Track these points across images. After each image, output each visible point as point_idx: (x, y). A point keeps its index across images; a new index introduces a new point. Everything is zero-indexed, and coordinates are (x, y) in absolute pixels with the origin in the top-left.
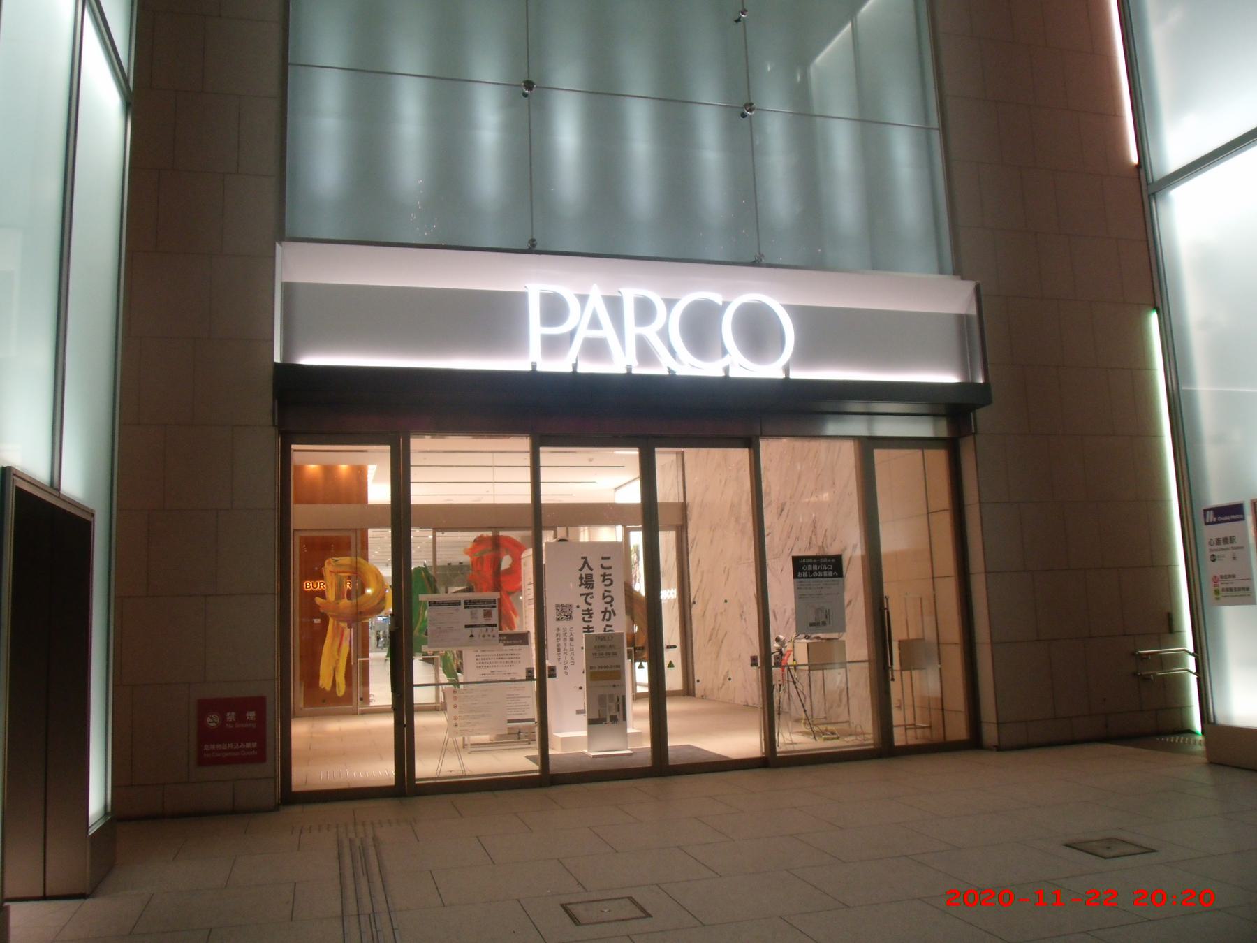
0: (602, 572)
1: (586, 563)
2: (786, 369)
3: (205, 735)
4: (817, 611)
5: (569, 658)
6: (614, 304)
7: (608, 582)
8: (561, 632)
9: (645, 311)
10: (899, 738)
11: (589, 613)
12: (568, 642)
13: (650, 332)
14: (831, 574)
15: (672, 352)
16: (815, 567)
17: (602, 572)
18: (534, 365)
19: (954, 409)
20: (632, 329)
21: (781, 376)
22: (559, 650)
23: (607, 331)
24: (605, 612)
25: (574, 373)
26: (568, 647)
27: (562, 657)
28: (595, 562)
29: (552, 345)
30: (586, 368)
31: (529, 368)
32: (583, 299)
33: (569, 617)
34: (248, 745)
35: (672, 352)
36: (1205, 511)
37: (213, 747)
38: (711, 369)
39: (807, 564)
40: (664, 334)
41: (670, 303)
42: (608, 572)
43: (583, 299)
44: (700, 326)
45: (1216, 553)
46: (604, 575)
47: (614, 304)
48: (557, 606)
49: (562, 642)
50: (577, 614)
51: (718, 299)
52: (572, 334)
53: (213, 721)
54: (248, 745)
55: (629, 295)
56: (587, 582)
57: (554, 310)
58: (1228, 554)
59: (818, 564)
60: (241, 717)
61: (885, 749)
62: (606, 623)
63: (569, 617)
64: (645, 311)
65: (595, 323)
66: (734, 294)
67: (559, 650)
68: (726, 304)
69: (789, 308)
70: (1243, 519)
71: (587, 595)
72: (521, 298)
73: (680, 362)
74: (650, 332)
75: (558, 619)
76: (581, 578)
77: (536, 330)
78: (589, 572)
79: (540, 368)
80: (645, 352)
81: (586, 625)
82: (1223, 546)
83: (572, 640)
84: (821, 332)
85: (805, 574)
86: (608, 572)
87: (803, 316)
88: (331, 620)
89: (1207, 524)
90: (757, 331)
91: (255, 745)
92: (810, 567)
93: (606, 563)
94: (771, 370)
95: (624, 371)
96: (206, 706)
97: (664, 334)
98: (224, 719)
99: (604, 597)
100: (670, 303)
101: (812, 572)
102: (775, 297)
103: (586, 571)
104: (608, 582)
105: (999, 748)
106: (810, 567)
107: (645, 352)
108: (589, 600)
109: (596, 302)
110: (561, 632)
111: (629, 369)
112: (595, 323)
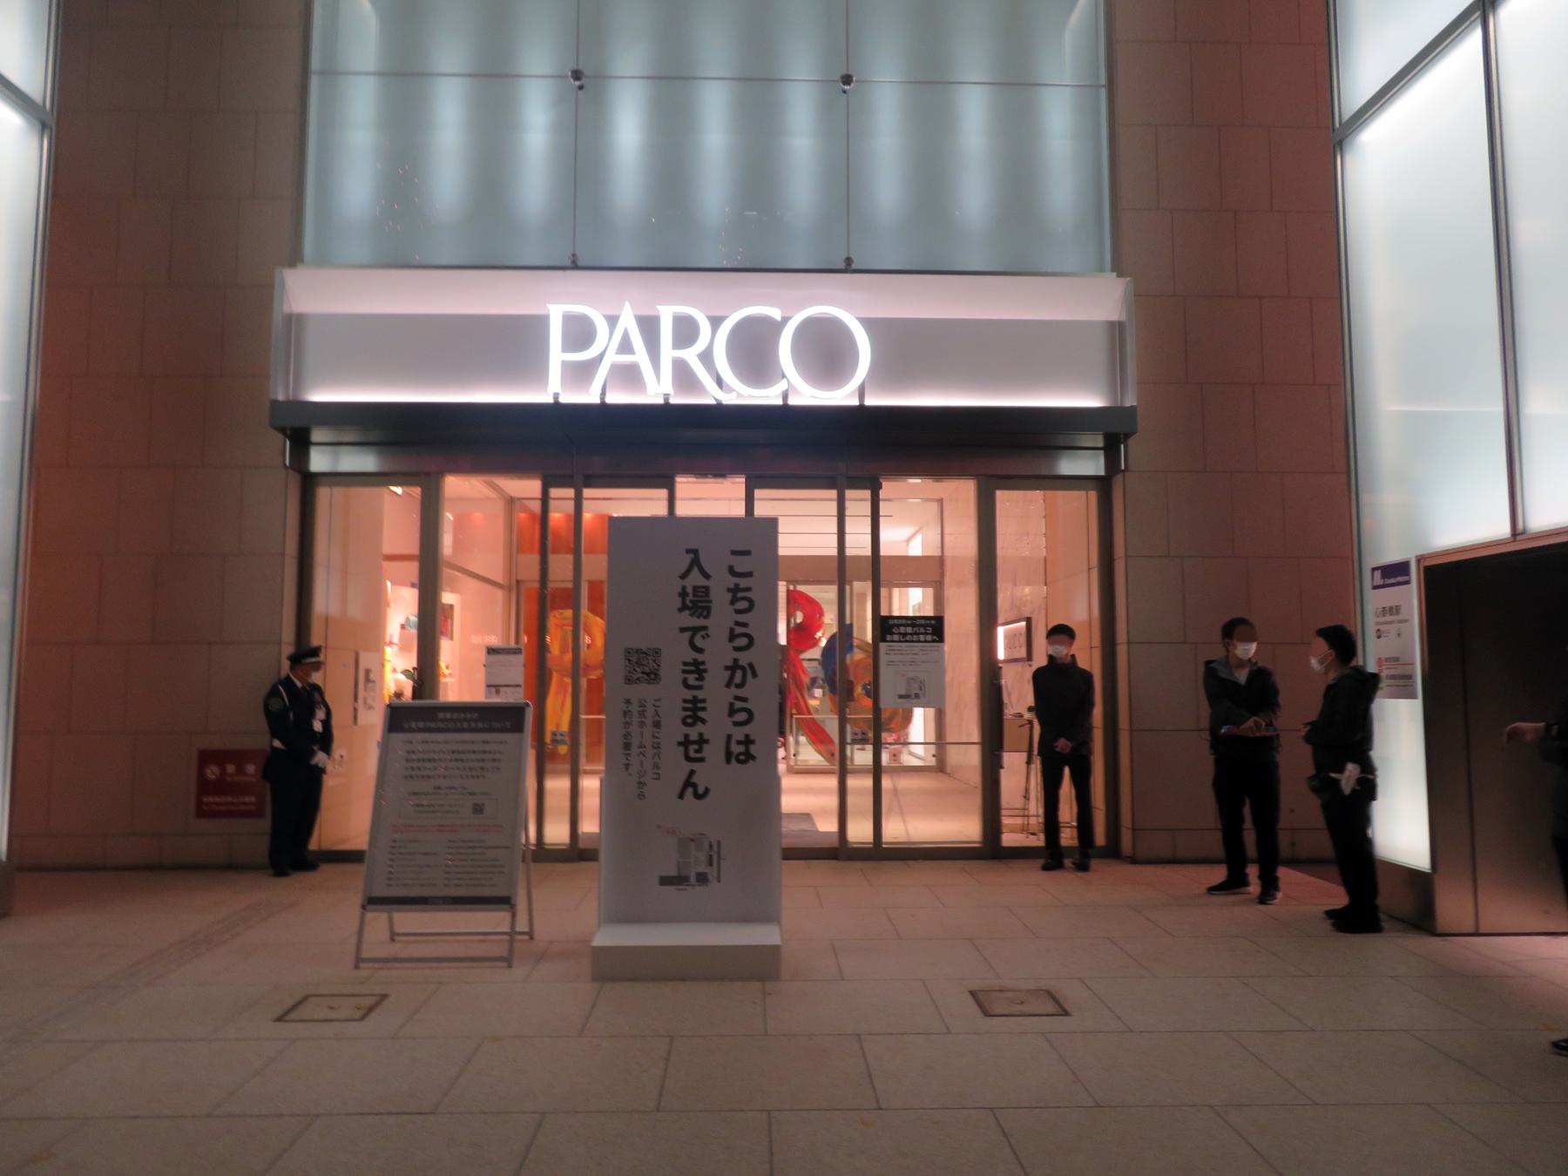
1: (695, 562)
2: (861, 392)
3: (205, 787)
4: (910, 680)
6: (649, 326)
7: (743, 605)
8: (634, 708)
9: (686, 332)
10: (1009, 839)
12: (649, 730)
13: (690, 355)
14: (929, 638)
15: (720, 382)
16: (909, 630)
18: (556, 396)
19: (1112, 429)
20: (668, 352)
21: (855, 402)
22: (627, 746)
24: (734, 667)
26: (648, 741)
28: (716, 562)
29: (580, 373)
30: (616, 398)
31: (550, 400)
32: (612, 321)
33: (653, 676)
34: (247, 799)
35: (720, 382)
36: (1374, 569)
37: (211, 799)
38: (769, 396)
39: (899, 626)
40: (706, 357)
41: (716, 322)
42: (743, 583)
43: (612, 321)
44: (753, 349)
45: (1382, 627)
46: (735, 590)
47: (649, 326)
48: (628, 652)
49: (634, 730)
50: (671, 671)
51: (776, 314)
52: (601, 356)
53: (212, 772)
54: (247, 799)
55: (666, 315)
56: (697, 602)
57: (580, 332)
58: (1393, 628)
59: (913, 625)
60: (241, 771)
61: (991, 850)
62: (734, 691)
63: (653, 676)
64: (686, 332)
65: (626, 346)
66: (790, 308)
67: (627, 746)
68: (785, 320)
69: (867, 323)
70: (1408, 582)
72: (542, 322)
73: (730, 390)
74: (690, 355)
75: (628, 681)
76: (683, 594)
77: (557, 356)
78: (701, 581)
80: (684, 376)
81: (689, 694)
82: (1388, 618)
83: (657, 725)
84: (903, 347)
85: (896, 637)
86: (743, 583)
88: (555, 676)
89: (1375, 588)
90: (825, 350)
91: (253, 799)
92: (902, 630)
93: (741, 564)
94: (842, 396)
95: (661, 401)
96: (206, 757)
98: (223, 769)
100: (716, 322)
101: (905, 635)
102: (848, 308)
103: (696, 579)
104: (743, 605)
105: (1134, 861)
106: (902, 630)
107: (684, 376)
108: (698, 642)
109: (628, 321)
111: (666, 397)
112: (626, 346)
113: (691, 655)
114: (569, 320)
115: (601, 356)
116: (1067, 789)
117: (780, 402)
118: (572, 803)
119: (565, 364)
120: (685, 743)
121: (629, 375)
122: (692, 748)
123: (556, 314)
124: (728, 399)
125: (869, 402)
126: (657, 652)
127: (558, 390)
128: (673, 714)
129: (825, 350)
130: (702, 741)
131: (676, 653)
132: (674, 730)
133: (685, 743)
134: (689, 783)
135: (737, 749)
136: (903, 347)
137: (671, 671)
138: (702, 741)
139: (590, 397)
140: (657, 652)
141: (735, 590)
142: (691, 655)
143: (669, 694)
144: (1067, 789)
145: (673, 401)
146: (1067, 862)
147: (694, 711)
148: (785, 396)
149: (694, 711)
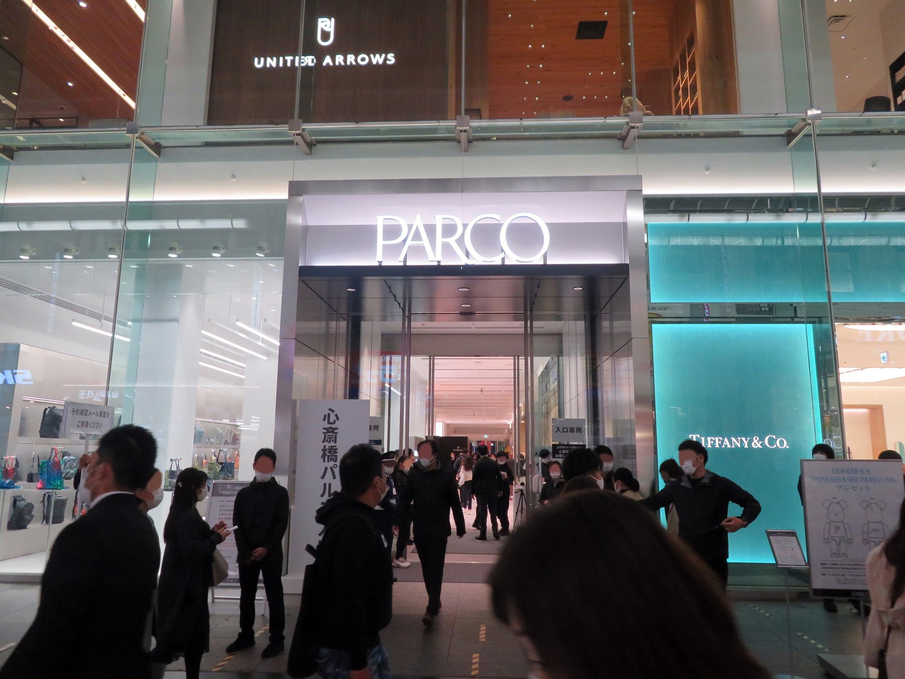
15: (467, 255)
20: (439, 239)
21: (542, 263)
23: (425, 241)
31: (377, 264)
40: (460, 241)
41: (465, 226)
55: (439, 222)
72: (372, 230)
74: (452, 241)
77: (380, 242)
80: (447, 248)
87: (552, 227)
97: (460, 241)
107: (447, 248)
112: (417, 236)
115: (405, 241)
116: (261, 595)
117: (500, 263)
118: (464, 476)
119: (385, 246)
121: (420, 250)
123: (380, 222)
125: (549, 262)
127: (381, 260)
129: (525, 234)
136: (564, 234)
139: (397, 262)
144: (261, 595)
145: (442, 264)
146: (311, 372)
148: (503, 259)
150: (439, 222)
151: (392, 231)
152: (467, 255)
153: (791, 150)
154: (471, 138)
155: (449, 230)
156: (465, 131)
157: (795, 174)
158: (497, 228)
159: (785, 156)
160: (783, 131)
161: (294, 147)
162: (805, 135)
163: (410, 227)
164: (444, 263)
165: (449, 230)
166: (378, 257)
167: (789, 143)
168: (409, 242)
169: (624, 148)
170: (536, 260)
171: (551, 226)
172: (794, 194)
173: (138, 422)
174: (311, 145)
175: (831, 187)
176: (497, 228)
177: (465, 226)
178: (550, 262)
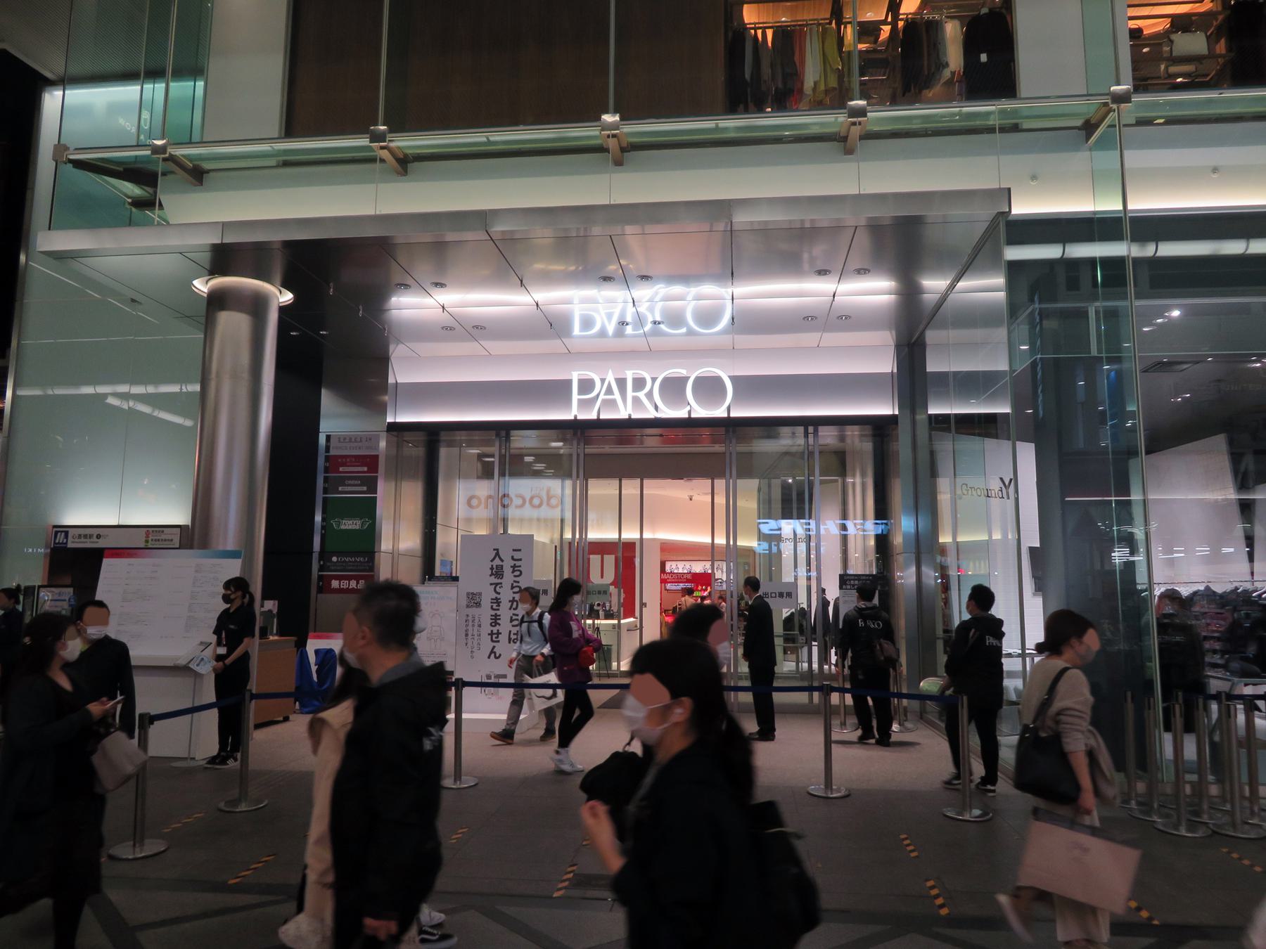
0: (513, 563)
1: (497, 554)
2: (729, 410)
5: (475, 642)
6: (621, 383)
8: (470, 618)
11: (497, 601)
12: (476, 628)
15: (656, 408)
17: (513, 563)
20: (630, 393)
21: (725, 415)
23: (617, 395)
25: (690, 418)
26: (476, 633)
27: (470, 642)
28: (506, 554)
33: (478, 605)
40: (650, 395)
41: (654, 380)
42: (518, 563)
46: (514, 567)
47: (621, 383)
49: (470, 628)
50: (486, 602)
51: (683, 372)
55: (629, 375)
56: (498, 572)
57: (586, 385)
63: (478, 605)
65: (609, 391)
69: (733, 378)
71: (497, 584)
72: (568, 383)
74: (641, 394)
76: (492, 568)
77: (575, 396)
79: (633, 417)
80: (637, 401)
81: (493, 613)
86: (518, 563)
87: (735, 380)
97: (650, 395)
99: (513, 587)
103: (497, 562)
107: (637, 401)
110: (470, 618)
112: (609, 391)
113: (495, 595)
114: (581, 382)
119: (579, 401)
120: (491, 634)
121: (611, 404)
122: (495, 636)
123: (575, 377)
124: (659, 415)
126: (480, 594)
128: (486, 621)
130: (498, 633)
131: (488, 595)
132: (486, 628)
133: (491, 634)
134: (492, 652)
135: (513, 637)
136: (749, 387)
137: (486, 602)
138: (498, 633)
139: (592, 415)
140: (480, 594)
141: (514, 567)
142: (495, 595)
143: (485, 613)
147: (495, 620)
148: (690, 412)
149: (495, 620)
150: (629, 375)
151: (586, 385)
152: (656, 408)
153: (1090, 150)
154: (624, 144)
155: (639, 383)
156: (614, 136)
157: (1096, 181)
158: (684, 380)
159: (1080, 159)
160: (1079, 123)
161: (378, 165)
162: (1110, 126)
163: (603, 381)
164: (635, 416)
165: (639, 383)
166: (573, 412)
167: (1088, 138)
168: (602, 397)
169: (849, 151)
170: (720, 413)
171: (734, 379)
172: (1095, 213)
173: (993, 589)
174: (405, 163)
175: (1145, 202)
176: (684, 380)
177: (654, 380)
178: (733, 414)
